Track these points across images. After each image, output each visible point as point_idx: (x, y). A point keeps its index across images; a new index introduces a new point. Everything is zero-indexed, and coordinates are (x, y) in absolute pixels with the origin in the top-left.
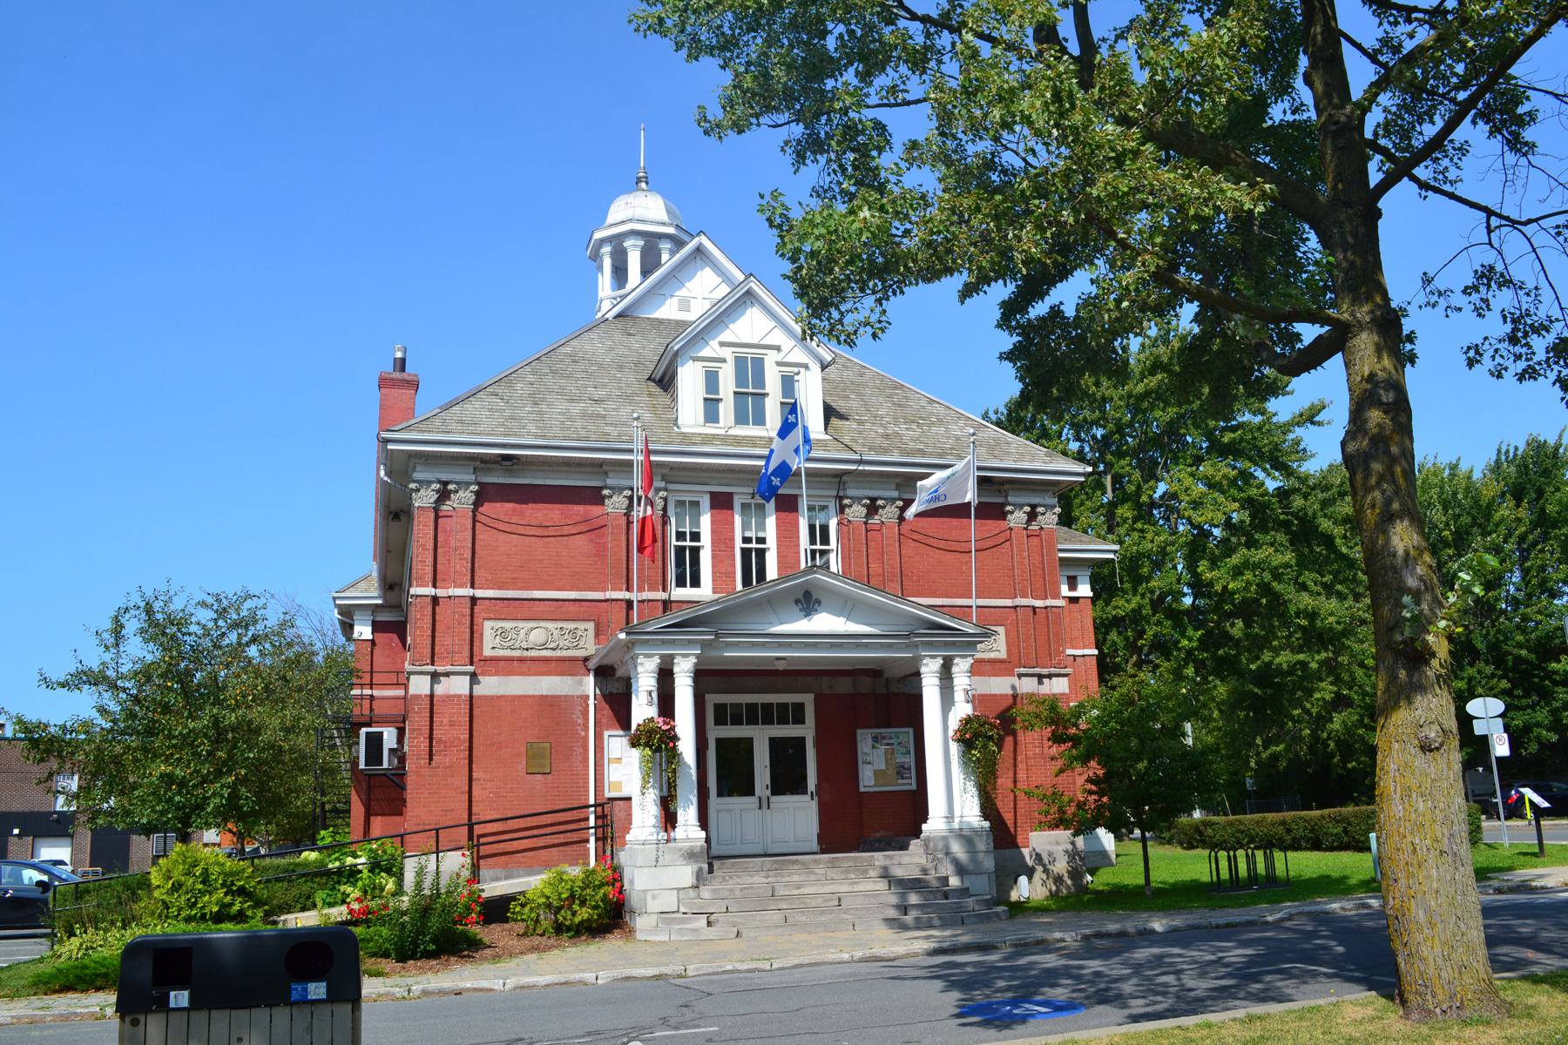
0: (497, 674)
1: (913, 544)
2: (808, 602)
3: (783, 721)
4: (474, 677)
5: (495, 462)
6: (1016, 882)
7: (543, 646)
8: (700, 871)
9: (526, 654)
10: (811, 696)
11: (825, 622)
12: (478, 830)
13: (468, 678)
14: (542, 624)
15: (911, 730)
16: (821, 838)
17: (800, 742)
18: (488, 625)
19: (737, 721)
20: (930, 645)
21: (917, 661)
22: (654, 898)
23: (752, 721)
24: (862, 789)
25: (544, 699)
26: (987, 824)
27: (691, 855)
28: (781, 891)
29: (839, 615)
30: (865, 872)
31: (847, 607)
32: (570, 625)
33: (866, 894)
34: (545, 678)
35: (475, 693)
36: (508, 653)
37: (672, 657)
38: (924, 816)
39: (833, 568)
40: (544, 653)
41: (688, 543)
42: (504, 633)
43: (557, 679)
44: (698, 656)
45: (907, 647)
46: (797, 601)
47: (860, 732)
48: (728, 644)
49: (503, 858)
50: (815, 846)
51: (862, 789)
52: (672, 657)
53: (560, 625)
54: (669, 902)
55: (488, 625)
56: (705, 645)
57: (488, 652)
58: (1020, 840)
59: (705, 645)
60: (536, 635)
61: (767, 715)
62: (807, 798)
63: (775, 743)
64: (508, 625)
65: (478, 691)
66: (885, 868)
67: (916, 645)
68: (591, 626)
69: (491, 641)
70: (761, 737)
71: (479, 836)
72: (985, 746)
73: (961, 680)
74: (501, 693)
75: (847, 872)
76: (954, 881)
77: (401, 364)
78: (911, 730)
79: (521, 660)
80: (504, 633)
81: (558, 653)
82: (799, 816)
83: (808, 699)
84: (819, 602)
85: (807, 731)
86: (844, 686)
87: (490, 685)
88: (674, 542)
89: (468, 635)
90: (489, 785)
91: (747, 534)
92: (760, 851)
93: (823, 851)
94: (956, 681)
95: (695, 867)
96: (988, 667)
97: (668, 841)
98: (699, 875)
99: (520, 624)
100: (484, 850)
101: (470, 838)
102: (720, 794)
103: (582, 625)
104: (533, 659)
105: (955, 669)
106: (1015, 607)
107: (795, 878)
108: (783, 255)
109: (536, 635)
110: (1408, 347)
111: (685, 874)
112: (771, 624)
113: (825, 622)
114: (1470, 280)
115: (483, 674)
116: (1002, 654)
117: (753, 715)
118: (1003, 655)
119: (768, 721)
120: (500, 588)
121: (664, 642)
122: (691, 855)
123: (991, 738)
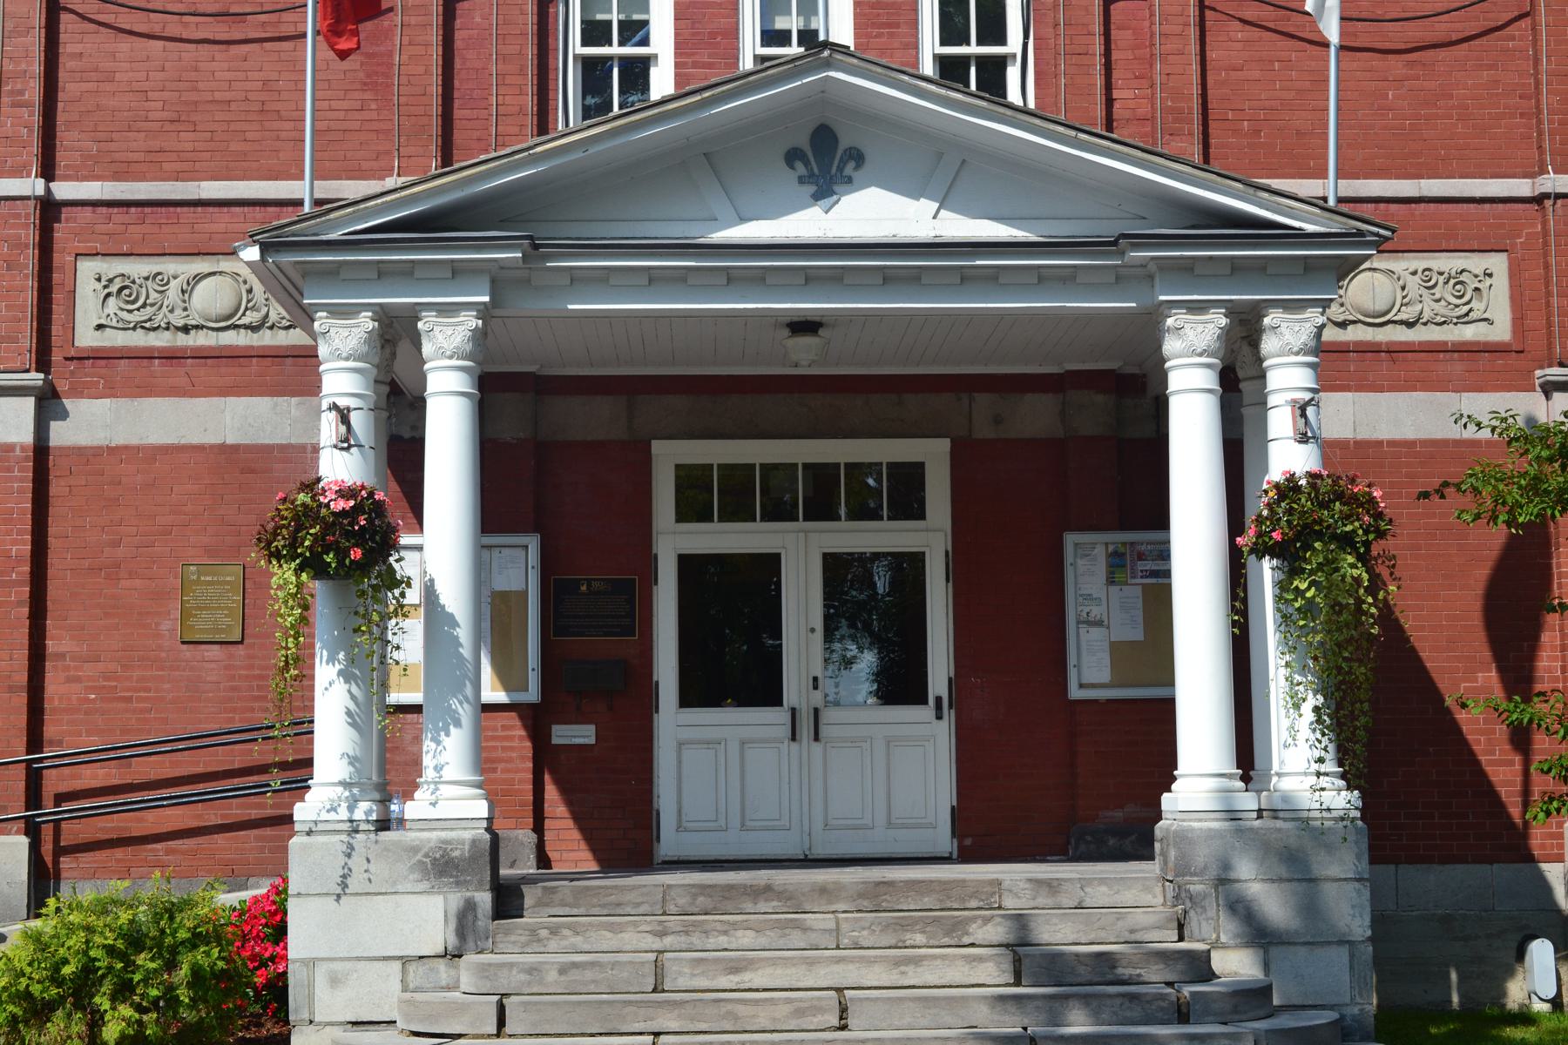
0: (111, 391)
1: (1240, 33)
2: (825, 155)
3: (864, 512)
4: (48, 404)
6: (1521, 955)
7: (227, 322)
8: (469, 908)
9: (182, 340)
10: (944, 445)
11: (871, 213)
12: (54, 782)
13: (30, 402)
16: (959, 817)
17: (909, 568)
18: (88, 269)
19: (738, 510)
20: (1187, 272)
21: (1149, 327)
22: (335, 981)
23: (778, 512)
24: (1075, 693)
25: (228, 454)
27: (442, 867)
28: (681, 976)
29: (915, 193)
30: (958, 926)
31: (943, 169)
33: (931, 1000)
34: (232, 401)
35: (61, 435)
36: (138, 339)
37: (411, 316)
38: (1163, 769)
39: (1013, 95)
41: (615, 49)
42: (124, 290)
43: (261, 405)
44: (484, 312)
45: (1120, 280)
46: (793, 156)
47: (1070, 539)
48: (575, 277)
49: (119, 853)
50: (944, 842)
51: (1075, 693)
52: (411, 316)
54: (381, 992)
55: (88, 269)
56: (499, 281)
57: (86, 338)
58: (1537, 840)
59: (499, 281)
61: (823, 495)
62: (925, 713)
63: (837, 569)
64: (137, 268)
65: (61, 435)
66: (1020, 921)
67: (1147, 276)
69: (91, 319)
70: (800, 553)
71: (60, 798)
72: (1330, 566)
73: (1286, 378)
74: (119, 439)
75: (905, 926)
76: (1236, 965)
79: (171, 356)
80: (124, 290)
81: (266, 339)
82: (908, 762)
83: (934, 454)
84: (857, 157)
85: (930, 537)
86: (1036, 418)
87: (89, 422)
88: (577, 47)
89: (30, 297)
90: (89, 670)
91: (780, 23)
92: (793, 850)
93: (967, 855)
94: (1275, 379)
95: (456, 899)
96: (1457, 367)
97: (383, 824)
98: (464, 921)
99: (169, 266)
100: (73, 832)
101: (33, 797)
102: (688, 699)
105: (1269, 344)
106: (1539, 200)
107: (746, 938)
111: (426, 918)
112: (715, 221)
113: (871, 213)
115: (77, 392)
116: (1501, 331)
117: (769, 496)
118: (1501, 331)
119: (821, 509)
120: (117, 176)
121: (383, 273)
122: (442, 867)
123: (1347, 541)
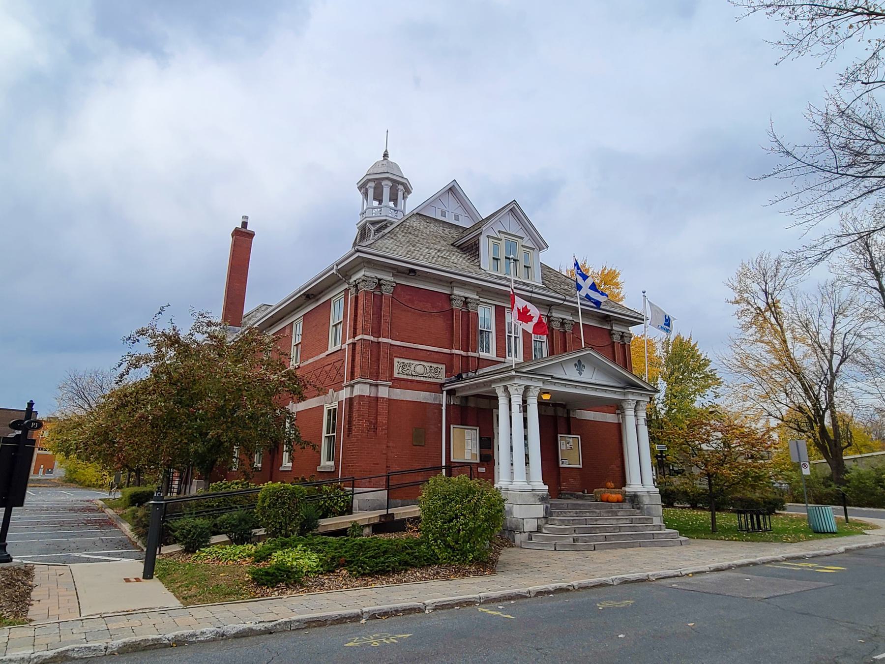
5: (447, 282)
9: (414, 378)
14: (422, 363)
15: (452, 460)
26: (547, 487)
32: (435, 365)
36: (405, 377)
40: (422, 379)
53: (430, 364)
60: (419, 369)
64: (406, 361)
68: (444, 367)
77: (245, 224)
78: (452, 460)
99: (412, 362)
103: (440, 366)
104: (417, 382)
108: (363, 233)
109: (419, 369)
110: (202, 407)
114: (35, 408)
